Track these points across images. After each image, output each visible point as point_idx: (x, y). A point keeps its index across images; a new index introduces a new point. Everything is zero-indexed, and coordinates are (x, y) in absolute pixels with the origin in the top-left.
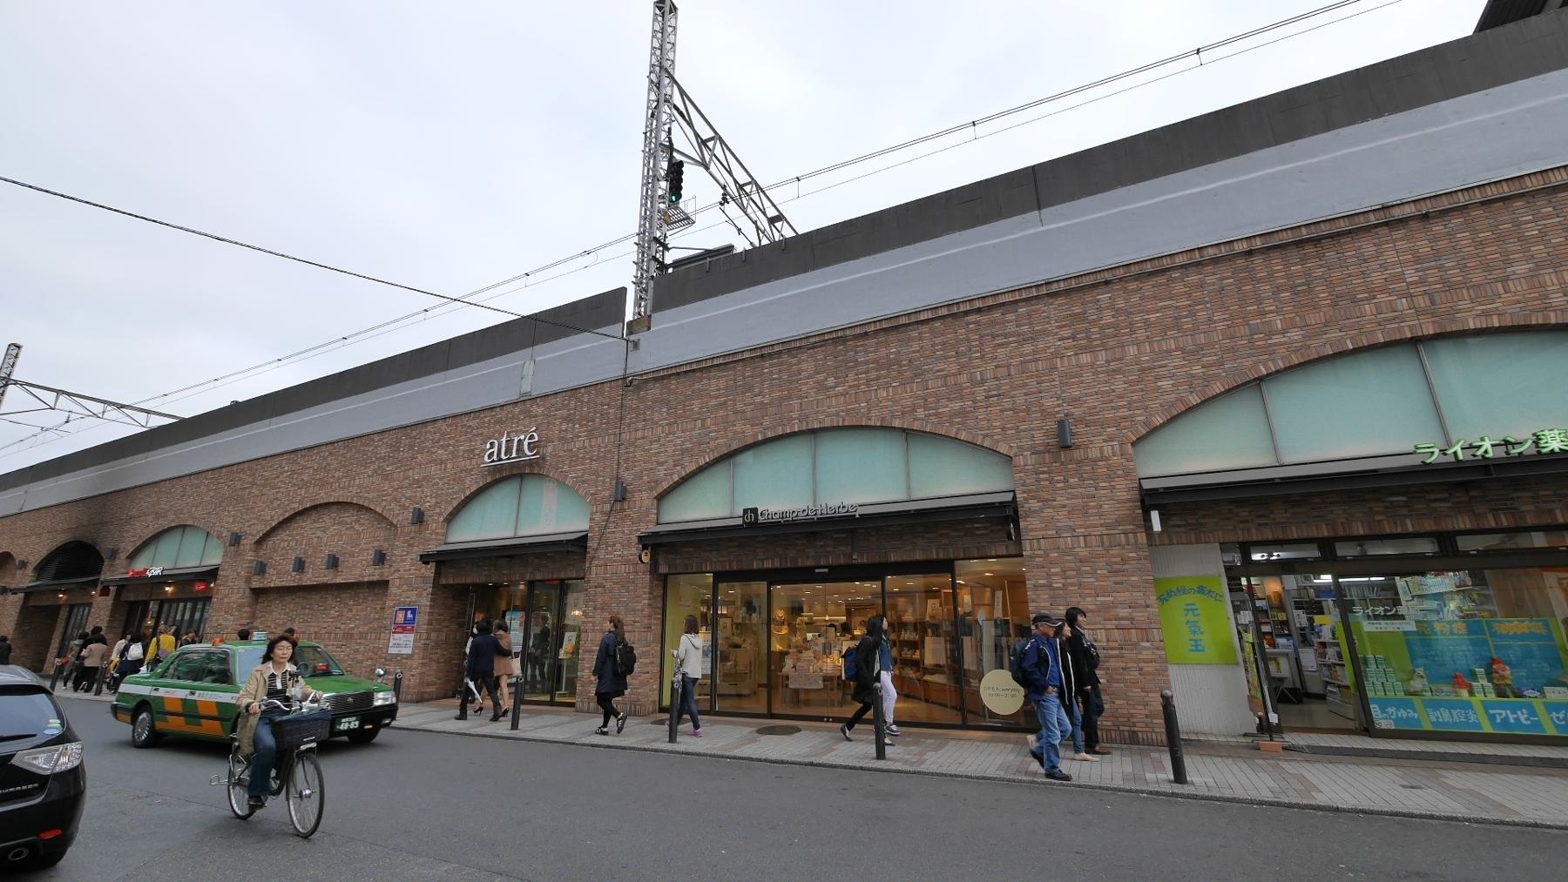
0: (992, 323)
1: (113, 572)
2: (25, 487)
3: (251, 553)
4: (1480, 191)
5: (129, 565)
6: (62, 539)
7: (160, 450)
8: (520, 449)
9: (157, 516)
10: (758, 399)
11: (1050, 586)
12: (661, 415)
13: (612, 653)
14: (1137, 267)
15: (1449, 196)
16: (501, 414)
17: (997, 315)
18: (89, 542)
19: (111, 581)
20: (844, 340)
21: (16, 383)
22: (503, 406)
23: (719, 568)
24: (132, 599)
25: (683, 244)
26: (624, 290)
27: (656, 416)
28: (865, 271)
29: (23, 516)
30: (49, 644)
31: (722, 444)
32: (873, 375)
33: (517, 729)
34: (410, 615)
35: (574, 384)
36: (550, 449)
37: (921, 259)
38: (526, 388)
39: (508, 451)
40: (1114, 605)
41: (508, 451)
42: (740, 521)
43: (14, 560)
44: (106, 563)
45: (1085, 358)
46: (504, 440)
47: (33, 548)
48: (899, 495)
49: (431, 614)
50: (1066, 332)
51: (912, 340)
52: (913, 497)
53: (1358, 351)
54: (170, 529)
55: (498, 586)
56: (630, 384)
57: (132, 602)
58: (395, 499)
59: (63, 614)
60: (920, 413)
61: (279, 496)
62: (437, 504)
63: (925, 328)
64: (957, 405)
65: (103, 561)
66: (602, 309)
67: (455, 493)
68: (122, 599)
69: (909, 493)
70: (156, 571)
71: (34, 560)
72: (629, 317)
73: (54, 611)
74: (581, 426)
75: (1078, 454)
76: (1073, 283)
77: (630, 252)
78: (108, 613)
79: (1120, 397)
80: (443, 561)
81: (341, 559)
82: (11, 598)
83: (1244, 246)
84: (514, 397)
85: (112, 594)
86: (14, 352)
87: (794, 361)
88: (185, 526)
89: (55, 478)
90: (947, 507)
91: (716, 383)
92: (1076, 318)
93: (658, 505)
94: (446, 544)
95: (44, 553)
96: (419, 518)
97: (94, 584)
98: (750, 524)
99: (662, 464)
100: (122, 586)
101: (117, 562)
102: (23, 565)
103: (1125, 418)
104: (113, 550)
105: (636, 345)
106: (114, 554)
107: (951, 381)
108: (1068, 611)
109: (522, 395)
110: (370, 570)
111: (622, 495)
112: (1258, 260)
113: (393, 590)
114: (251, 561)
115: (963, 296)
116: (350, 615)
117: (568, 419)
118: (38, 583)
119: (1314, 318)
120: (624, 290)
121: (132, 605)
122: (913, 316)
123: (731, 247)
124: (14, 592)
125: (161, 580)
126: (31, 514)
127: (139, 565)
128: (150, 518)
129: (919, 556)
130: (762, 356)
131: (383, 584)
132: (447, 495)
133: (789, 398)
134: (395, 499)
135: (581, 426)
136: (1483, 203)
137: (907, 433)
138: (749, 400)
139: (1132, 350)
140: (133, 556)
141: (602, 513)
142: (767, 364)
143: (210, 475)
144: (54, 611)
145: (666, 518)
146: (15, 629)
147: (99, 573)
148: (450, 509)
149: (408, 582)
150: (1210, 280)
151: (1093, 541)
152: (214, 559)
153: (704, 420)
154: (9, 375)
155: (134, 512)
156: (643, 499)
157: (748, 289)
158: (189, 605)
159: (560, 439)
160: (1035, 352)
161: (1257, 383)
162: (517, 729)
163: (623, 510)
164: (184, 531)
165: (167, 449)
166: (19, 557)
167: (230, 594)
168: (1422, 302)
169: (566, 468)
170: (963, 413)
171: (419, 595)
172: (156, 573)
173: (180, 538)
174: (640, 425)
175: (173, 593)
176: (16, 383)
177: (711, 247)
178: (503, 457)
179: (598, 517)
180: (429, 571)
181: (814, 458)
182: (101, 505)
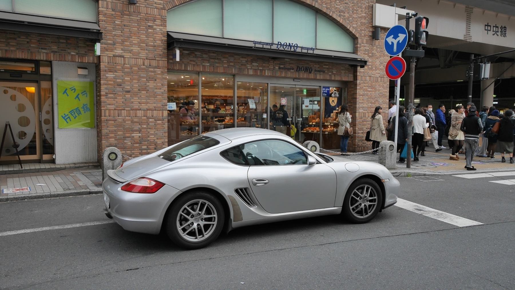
175: (223, 78)
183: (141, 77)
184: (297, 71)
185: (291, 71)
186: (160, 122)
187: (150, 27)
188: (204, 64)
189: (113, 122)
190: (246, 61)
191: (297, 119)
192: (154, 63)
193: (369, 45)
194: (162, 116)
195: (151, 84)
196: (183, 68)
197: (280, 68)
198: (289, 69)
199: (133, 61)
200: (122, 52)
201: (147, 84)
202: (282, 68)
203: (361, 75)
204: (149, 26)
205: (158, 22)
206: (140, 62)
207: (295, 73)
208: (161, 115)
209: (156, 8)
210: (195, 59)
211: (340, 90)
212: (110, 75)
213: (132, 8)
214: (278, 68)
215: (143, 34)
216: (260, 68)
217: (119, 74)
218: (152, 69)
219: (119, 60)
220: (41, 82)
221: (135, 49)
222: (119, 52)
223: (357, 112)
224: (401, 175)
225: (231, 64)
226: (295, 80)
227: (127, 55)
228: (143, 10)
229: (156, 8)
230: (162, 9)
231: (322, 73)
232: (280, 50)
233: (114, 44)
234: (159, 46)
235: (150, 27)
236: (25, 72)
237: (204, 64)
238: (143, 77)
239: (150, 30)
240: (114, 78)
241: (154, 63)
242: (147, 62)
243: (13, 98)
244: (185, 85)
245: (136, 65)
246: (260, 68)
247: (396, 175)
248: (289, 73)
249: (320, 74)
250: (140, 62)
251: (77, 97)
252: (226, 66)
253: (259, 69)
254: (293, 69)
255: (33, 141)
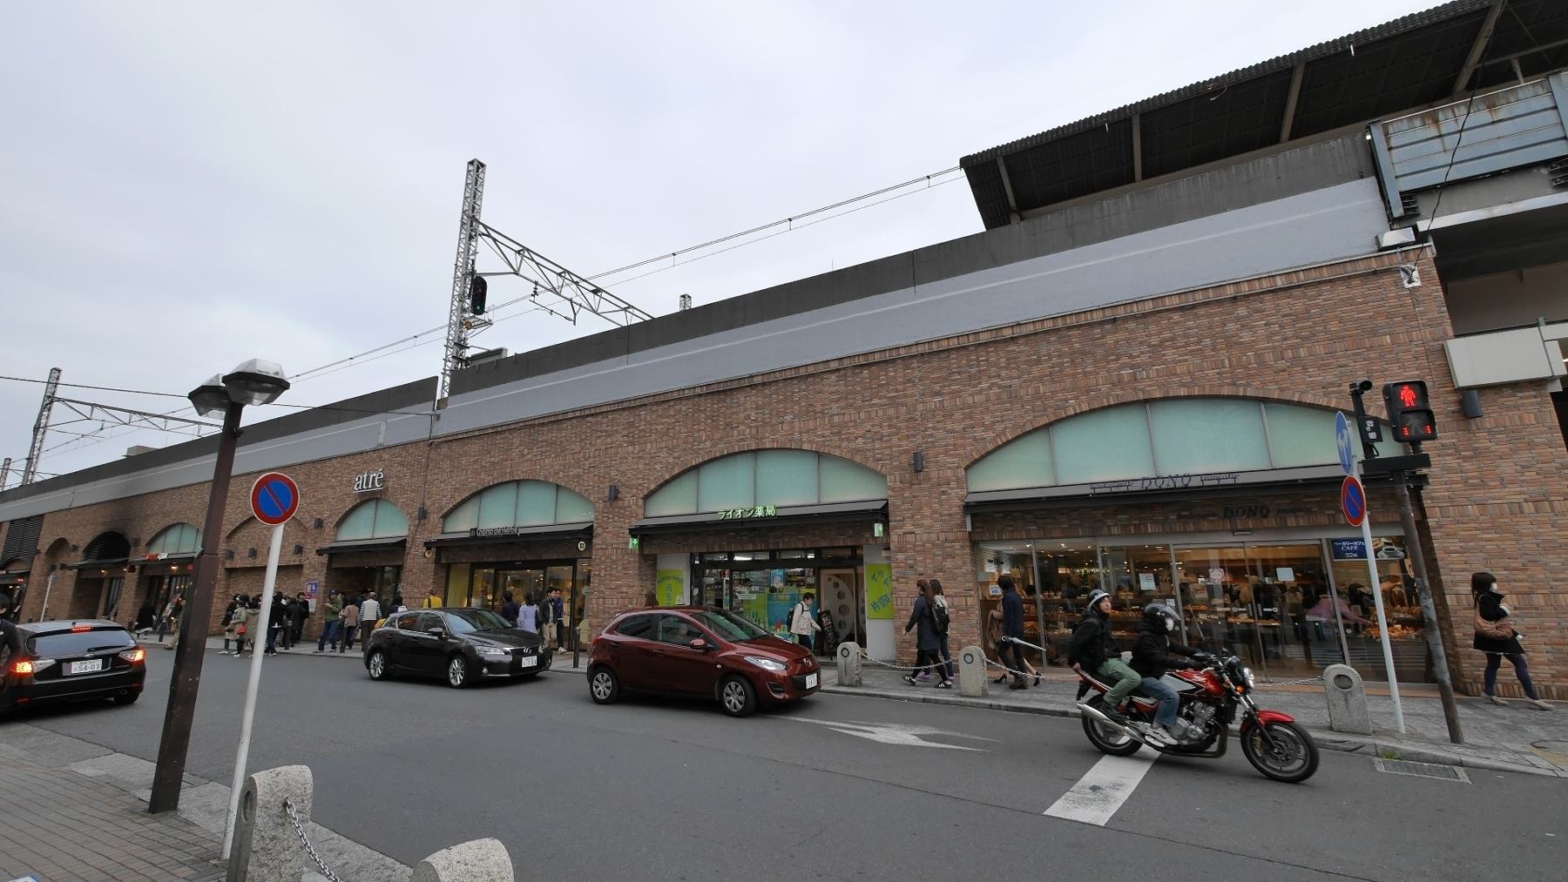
0: (596, 423)
1: (137, 557)
2: (72, 489)
3: (224, 544)
4: (1376, 262)
5: (147, 552)
6: (100, 530)
7: (550, 375)
8: (373, 483)
9: (165, 515)
10: (493, 459)
11: (599, 575)
12: (446, 465)
13: (927, 613)
14: (956, 341)
15: (1341, 266)
16: (366, 457)
17: (599, 418)
18: (121, 533)
19: (137, 562)
20: (532, 426)
21: (59, 400)
22: (949, 338)
23: (473, 561)
24: (151, 574)
25: (479, 342)
26: (437, 378)
27: (445, 466)
28: (552, 382)
29: (72, 511)
30: (98, 607)
31: (475, 486)
32: (544, 449)
33: (577, 667)
34: (314, 588)
35: (406, 440)
36: (391, 483)
37: (523, 390)
38: (381, 441)
39: (367, 484)
40: (621, 586)
41: (367, 484)
42: (468, 535)
43: (68, 543)
44: (132, 548)
45: (631, 449)
46: (365, 476)
47: (81, 536)
48: (510, 525)
49: (325, 586)
50: (625, 432)
51: (562, 429)
52: (700, 512)
53: (1092, 411)
54: (173, 526)
55: (372, 570)
56: (432, 443)
57: (151, 577)
58: (307, 511)
59: (106, 585)
60: (561, 474)
61: (240, 505)
62: (330, 516)
63: (569, 423)
64: (576, 471)
65: (130, 547)
66: (421, 391)
67: (339, 509)
68: (145, 574)
69: (697, 510)
70: (164, 556)
71: (83, 545)
72: (438, 397)
73: (99, 582)
74: (408, 469)
75: (620, 503)
76: (1211, 295)
77: (441, 353)
78: (135, 584)
79: (641, 472)
80: (334, 554)
81: (599, 531)
82: (69, 573)
83: (1230, 292)
84: (373, 446)
85: (137, 571)
86: (56, 375)
87: (511, 436)
88: (183, 524)
89: (92, 483)
90: (1290, 481)
91: (474, 447)
92: (631, 424)
93: (645, 504)
94: (645, 518)
95: (89, 540)
96: (319, 524)
97: (125, 563)
98: (473, 537)
99: (445, 496)
100: (143, 567)
101: (140, 548)
102: (75, 548)
103: (640, 484)
104: (136, 539)
105: (438, 417)
106: (137, 542)
107: (576, 456)
108: (1474, 576)
109: (380, 445)
110: (294, 557)
111: (423, 514)
112: (702, 399)
113: (306, 571)
114: (225, 550)
115: (1249, 275)
116: (285, 586)
117: (401, 464)
118: (86, 562)
119: (717, 435)
120: (437, 378)
121: (152, 578)
122: (632, 402)
123: (499, 351)
124: (70, 568)
125: (168, 562)
126: (78, 510)
127: (154, 551)
128: (159, 517)
129: (555, 557)
130: (496, 432)
131: (299, 567)
132: (336, 509)
133: (506, 460)
134: (307, 511)
135: (408, 469)
136: (784, 380)
137: (819, 455)
138: (488, 460)
139: (649, 446)
140: (150, 543)
141: (415, 526)
142: (498, 437)
143: (197, 487)
144: (99, 582)
145: (448, 529)
146: (73, 596)
147: (128, 556)
148: (337, 519)
149: (313, 566)
150: (684, 408)
151: (619, 551)
152: (574, 515)
153: (466, 471)
154: (53, 394)
155: (149, 512)
156: (630, 499)
157: (1056, 255)
158: (179, 579)
159: (396, 476)
160: (612, 443)
161: (697, 467)
162: (577, 667)
163: (424, 525)
164: (182, 529)
165: (166, 466)
166: (72, 543)
167: (418, 561)
168: (754, 431)
169: (399, 496)
170: (578, 476)
171: (319, 575)
172: (163, 557)
173: (374, 510)
174: (436, 471)
175: (177, 570)
176: (59, 400)
177: (491, 349)
178: (364, 487)
179: (412, 528)
180: (325, 559)
181: (1050, 443)
182: (126, 506)
183: (935, 555)
184: (1225, 516)
185: (1211, 518)
186: (964, 613)
187: (944, 493)
188: (1027, 528)
189: (905, 612)
190: (1103, 514)
191: (1260, 609)
192: (951, 536)
193: (1454, 433)
194: (967, 605)
195: (948, 564)
196: (1221, 528)
197: (1179, 517)
198: (1204, 517)
199: (925, 537)
200: (912, 527)
201: (944, 563)
202: (1186, 517)
203: (1440, 505)
204: (942, 491)
205: (953, 484)
206: (934, 536)
207: (1221, 522)
208: (964, 604)
209: (950, 468)
210: (1013, 523)
211: (141, 569)
212: (901, 556)
213: (921, 475)
214: (1175, 517)
215: (935, 503)
216: (1134, 522)
217: (911, 553)
218: (949, 544)
219: (910, 538)
220: (1278, 570)
221: (927, 522)
222: (909, 528)
223: (1446, 592)
224: (1360, 750)
225: (1074, 522)
226: (1236, 533)
227: (918, 531)
228: (934, 475)
229: (950, 468)
230: (957, 468)
231: (1302, 514)
232: (1163, 490)
233: (904, 520)
234: (956, 514)
235: (944, 493)
236: (843, 558)
237: (1027, 528)
238: (939, 555)
239: (944, 497)
240: (906, 559)
241: (951, 536)
242: (942, 536)
243: (836, 585)
244: (1072, 560)
245: (929, 541)
246: (1134, 522)
247: (1345, 746)
248: (1205, 523)
249: (1296, 517)
250: (934, 536)
251: (885, 582)
252: (1066, 526)
253: (1132, 525)
254: (1214, 515)
255: (852, 630)
